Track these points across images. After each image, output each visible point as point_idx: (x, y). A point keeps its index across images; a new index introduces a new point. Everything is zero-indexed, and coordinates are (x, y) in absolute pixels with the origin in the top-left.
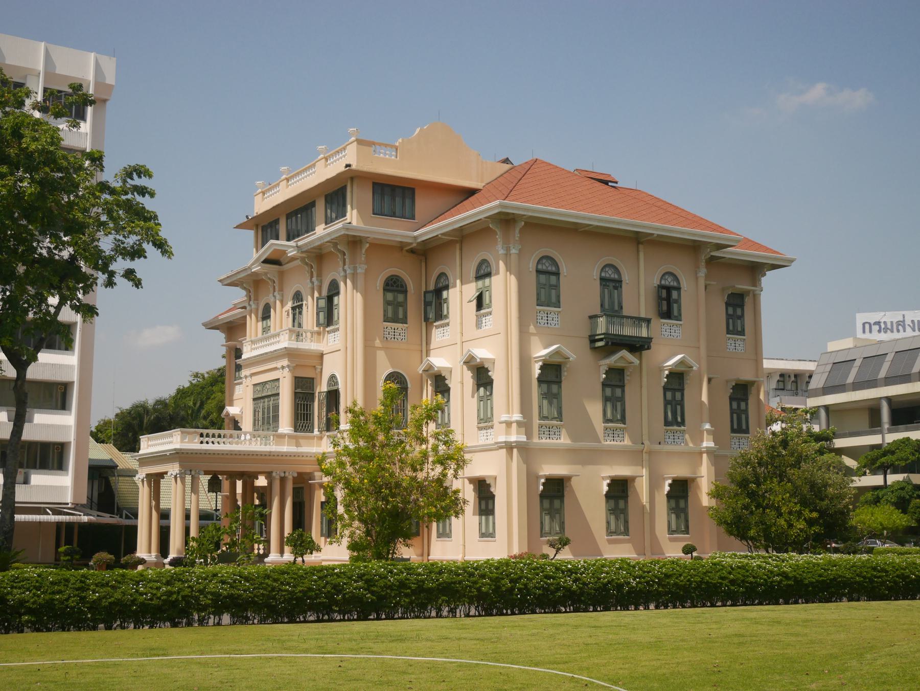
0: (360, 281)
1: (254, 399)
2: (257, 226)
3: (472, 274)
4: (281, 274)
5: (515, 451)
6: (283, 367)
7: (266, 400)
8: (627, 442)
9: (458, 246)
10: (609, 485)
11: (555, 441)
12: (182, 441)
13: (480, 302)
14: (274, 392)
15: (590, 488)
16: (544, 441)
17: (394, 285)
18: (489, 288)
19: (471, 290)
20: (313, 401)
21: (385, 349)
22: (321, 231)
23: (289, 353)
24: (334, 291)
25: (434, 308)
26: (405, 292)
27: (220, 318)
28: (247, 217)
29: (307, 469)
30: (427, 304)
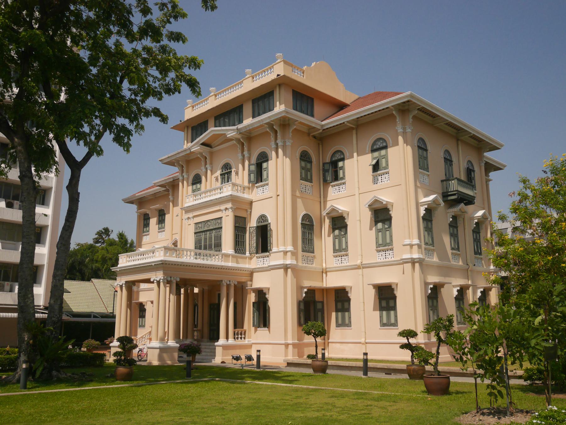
0: (289, 151)
1: (195, 233)
2: (188, 127)
3: (368, 148)
4: (211, 154)
5: (289, 270)
6: (226, 209)
7: (208, 233)
8: (461, 263)
9: (354, 132)
10: (458, 291)
11: (310, 265)
12: (165, 255)
13: (376, 167)
14: (217, 227)
15: (449, 294)
16: (304, 265)
17: (305, 157)
18: (386, 157)
19: (368, 160)
20: (246, 233)
21: (301, 197)
22: (248, 121)
23: (232, 199)
24: (263, 158)
25: (332, 172)
26: (311, 162)
27: (137, 195)
28: (181, 121)
29: (243, 279)
30: (325, 171)
